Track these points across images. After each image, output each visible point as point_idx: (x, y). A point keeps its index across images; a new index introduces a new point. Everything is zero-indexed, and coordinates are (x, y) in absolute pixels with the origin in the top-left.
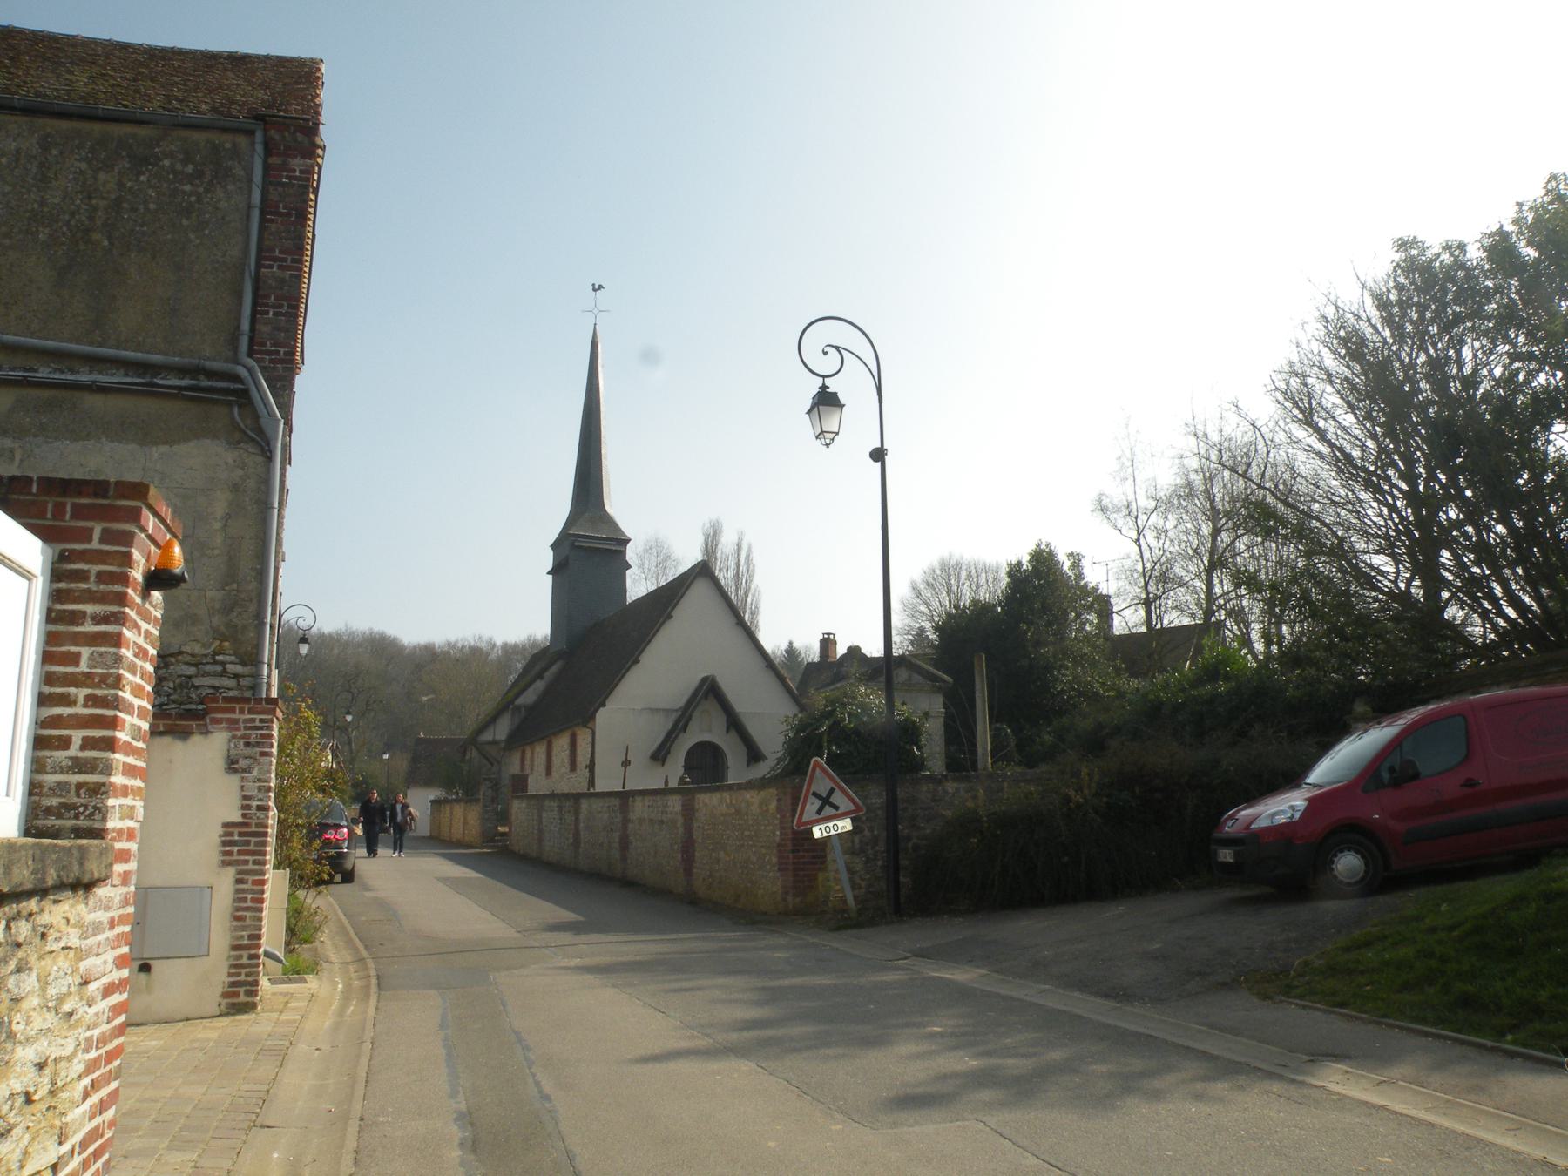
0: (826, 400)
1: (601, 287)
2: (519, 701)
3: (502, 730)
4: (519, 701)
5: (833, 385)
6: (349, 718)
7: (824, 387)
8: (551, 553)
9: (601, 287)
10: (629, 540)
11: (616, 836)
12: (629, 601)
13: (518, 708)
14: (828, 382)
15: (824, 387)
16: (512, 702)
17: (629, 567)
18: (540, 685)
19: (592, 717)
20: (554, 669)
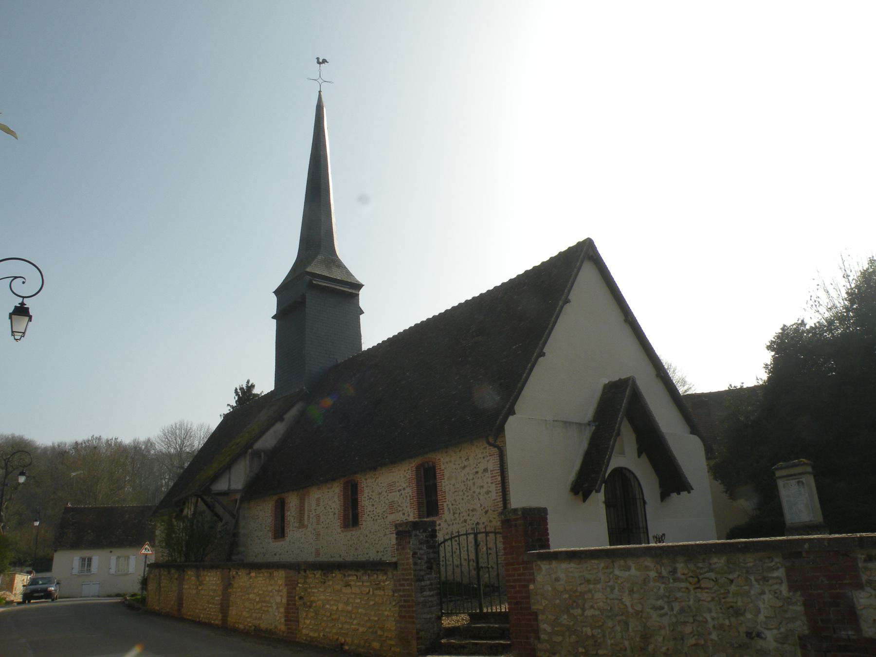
0: (21, 311)
1: (324, 61)
2: (258, 445)
3: (237, 479)
4: (258, 445)
5: (28, 303)
6: (22, 479)
7: (22, 304)
8: (274, 299)
9: (324, 61)
10: (359, 286)
11: (473, 565)
12: (366, 346)
13: (257, 454)
14: (26, 301)
15: (22, 304)
16: (250, 445)
17: (362, 312)
18: (279, 428)
19: (501, 430)
20: (294, 411)
